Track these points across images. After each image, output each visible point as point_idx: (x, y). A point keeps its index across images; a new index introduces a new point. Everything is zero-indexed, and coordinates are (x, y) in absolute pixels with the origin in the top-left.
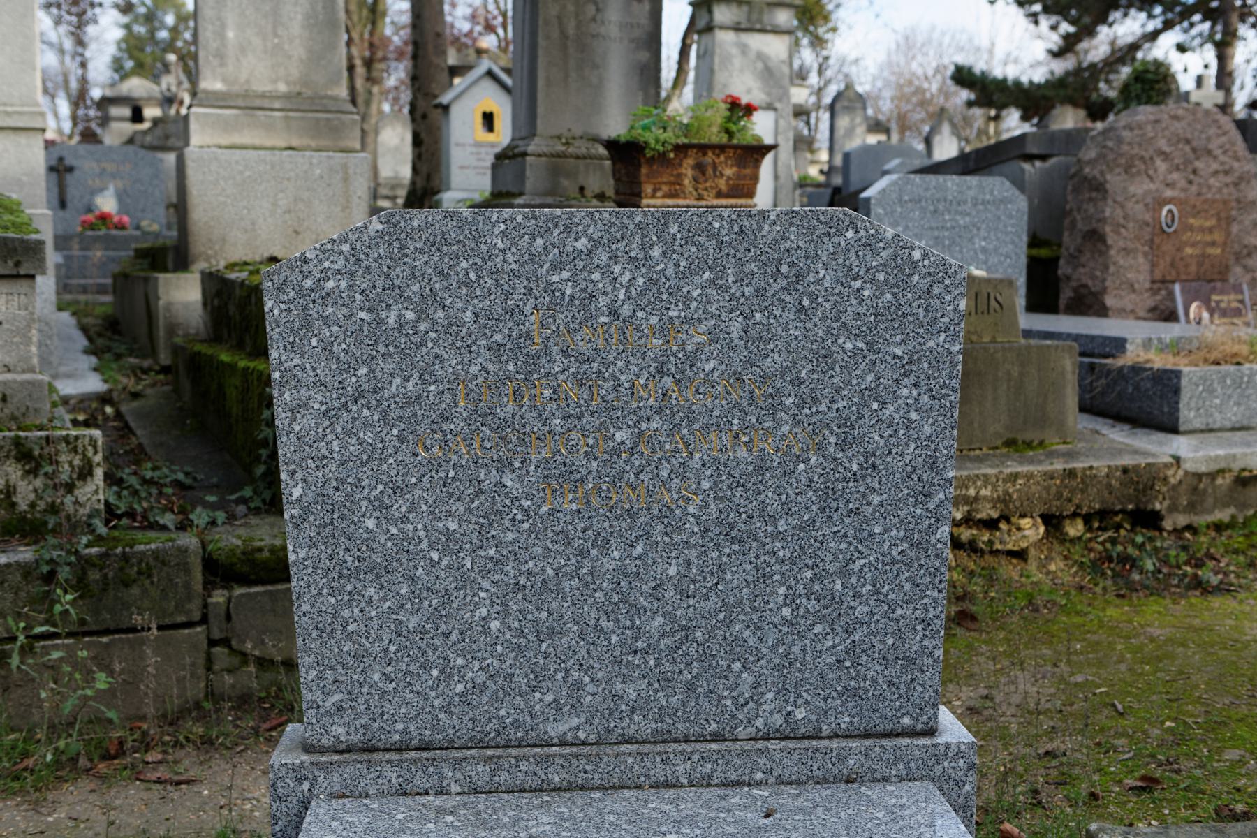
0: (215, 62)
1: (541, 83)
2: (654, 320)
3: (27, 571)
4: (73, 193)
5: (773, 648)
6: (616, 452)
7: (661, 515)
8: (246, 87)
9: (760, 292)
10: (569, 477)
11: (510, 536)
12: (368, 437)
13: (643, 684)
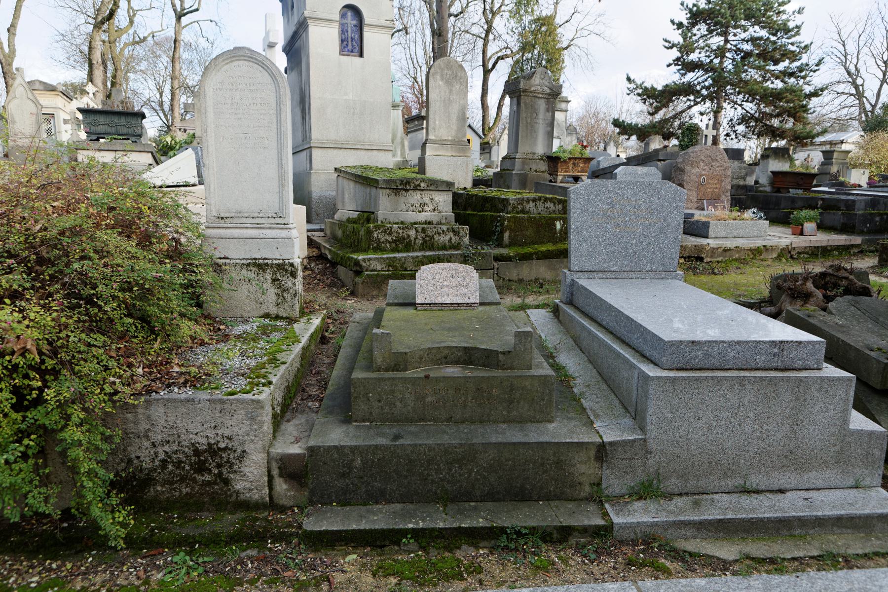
10: (618, 226)
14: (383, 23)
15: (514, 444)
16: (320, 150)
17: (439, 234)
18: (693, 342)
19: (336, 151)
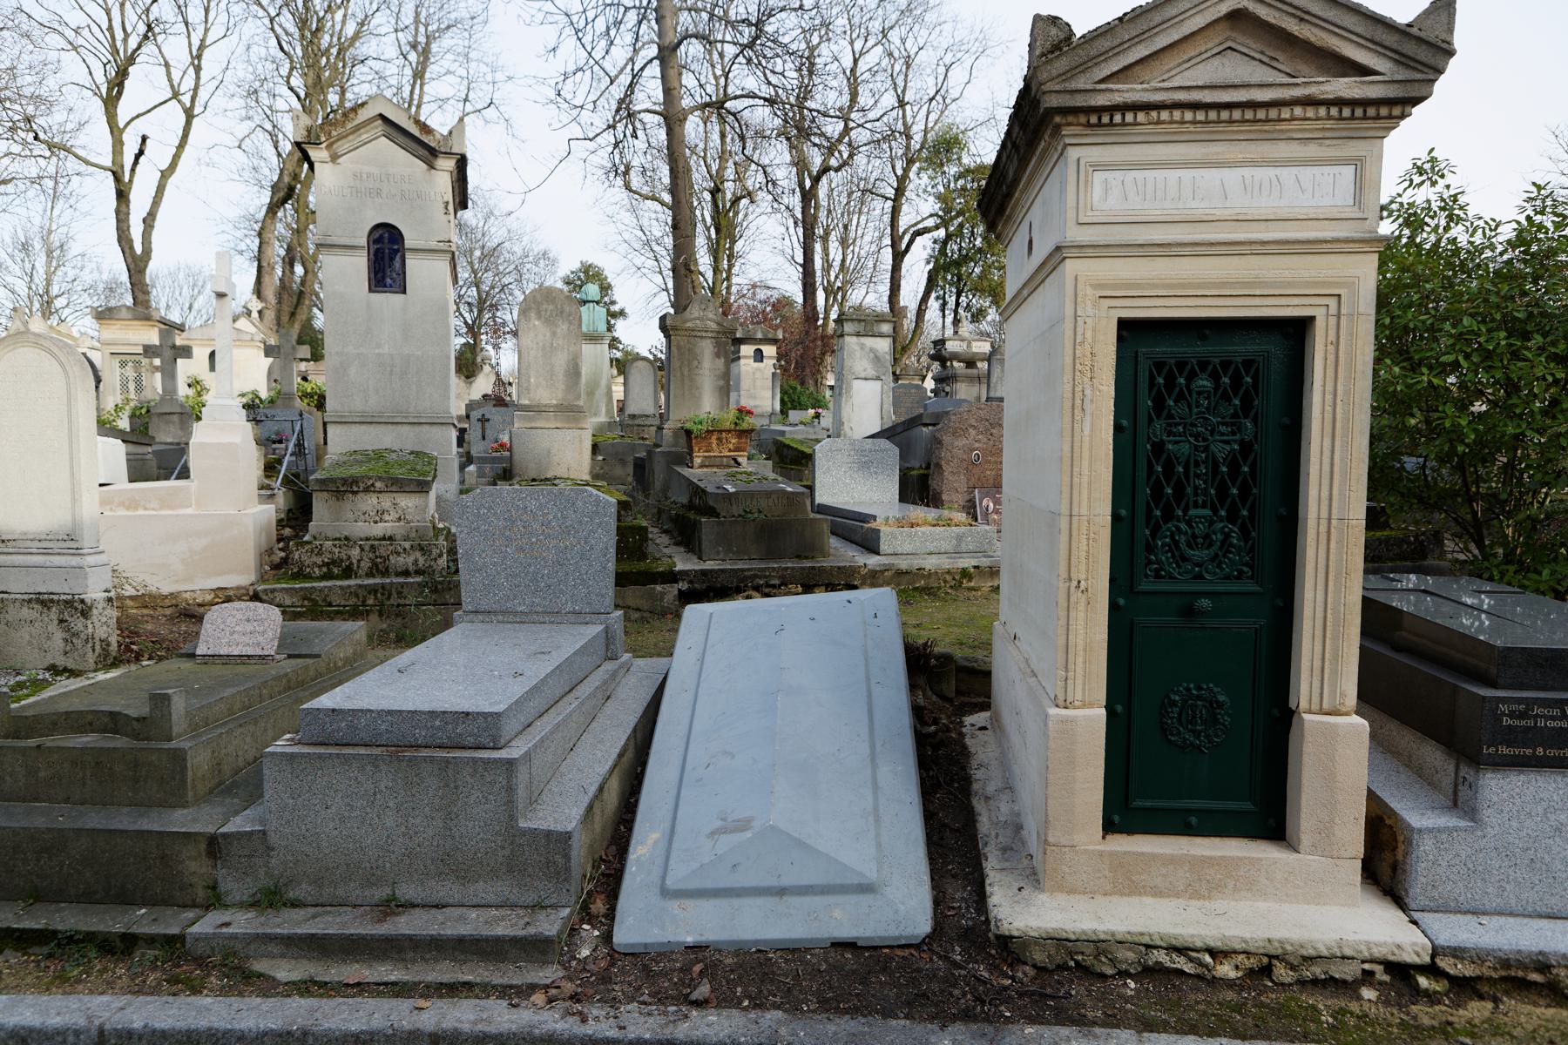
3: (419, 584)
4: (488, 433)
14: (433, 245)
15: (110, 831)
16: (340, 427)
17: (398, 554)
19: (363, 427)
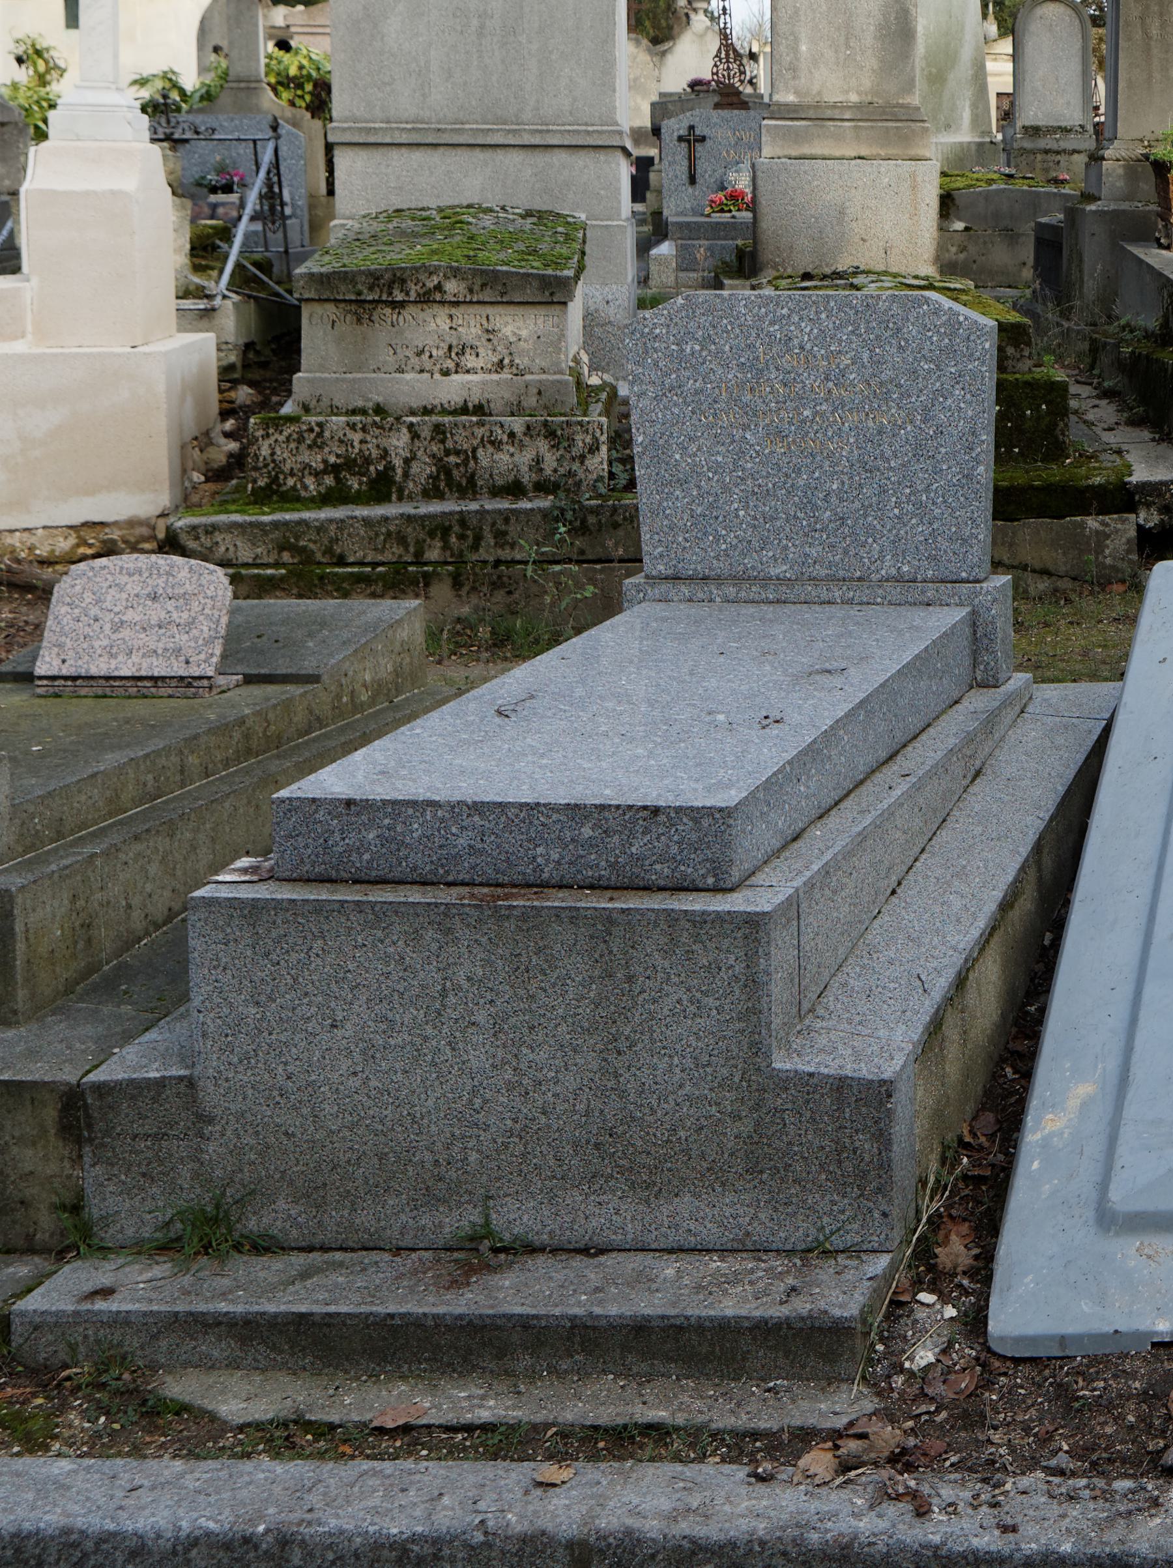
0: (789, 76)
1: (1121, 85)
2: (823, 352)
4: (702, 166)
5: (890, 531)
6: (804, 421)
7: (828, 456)
8: (818, 99)
9: (878, 337)
10: (780, 435)
11: (749, 465)
12: (676, 411)
13: (820, 548)
17: (497, 444)
18: (349, 803)
19: (417, 156)
